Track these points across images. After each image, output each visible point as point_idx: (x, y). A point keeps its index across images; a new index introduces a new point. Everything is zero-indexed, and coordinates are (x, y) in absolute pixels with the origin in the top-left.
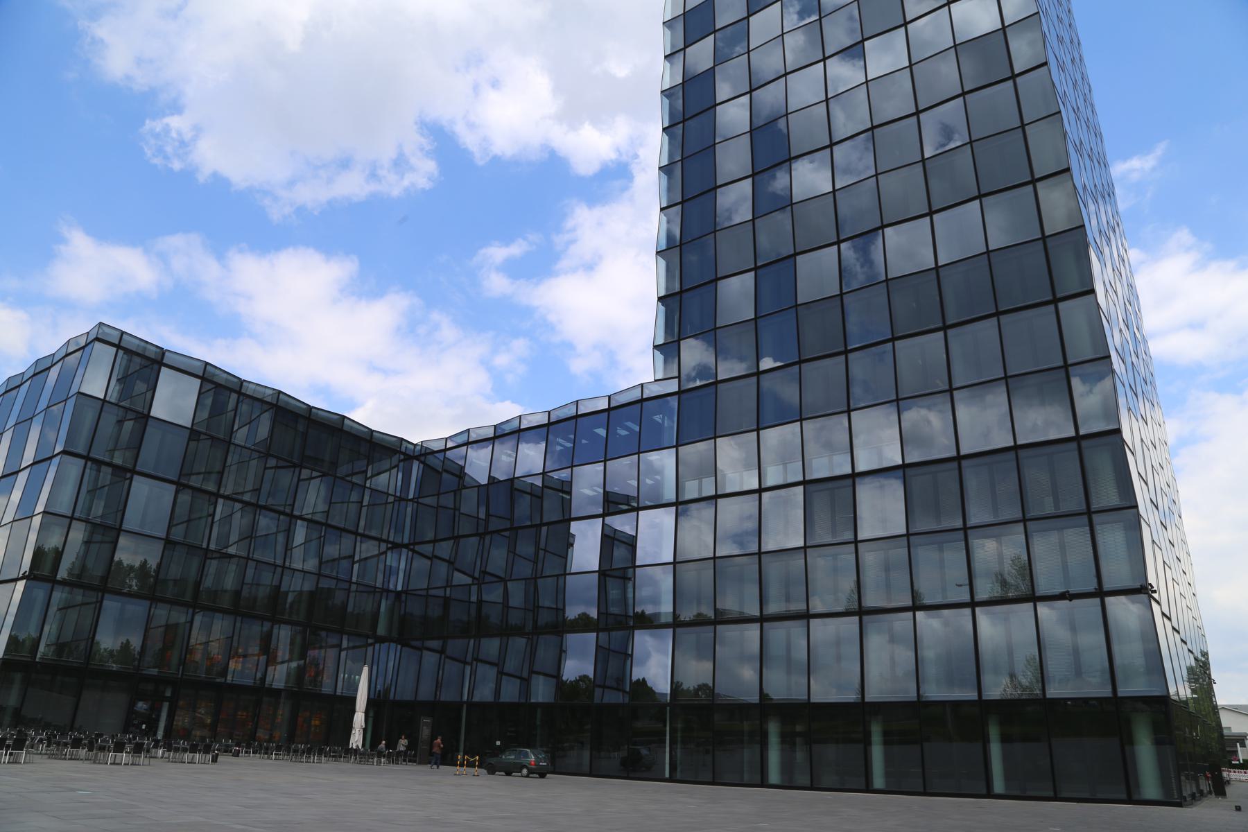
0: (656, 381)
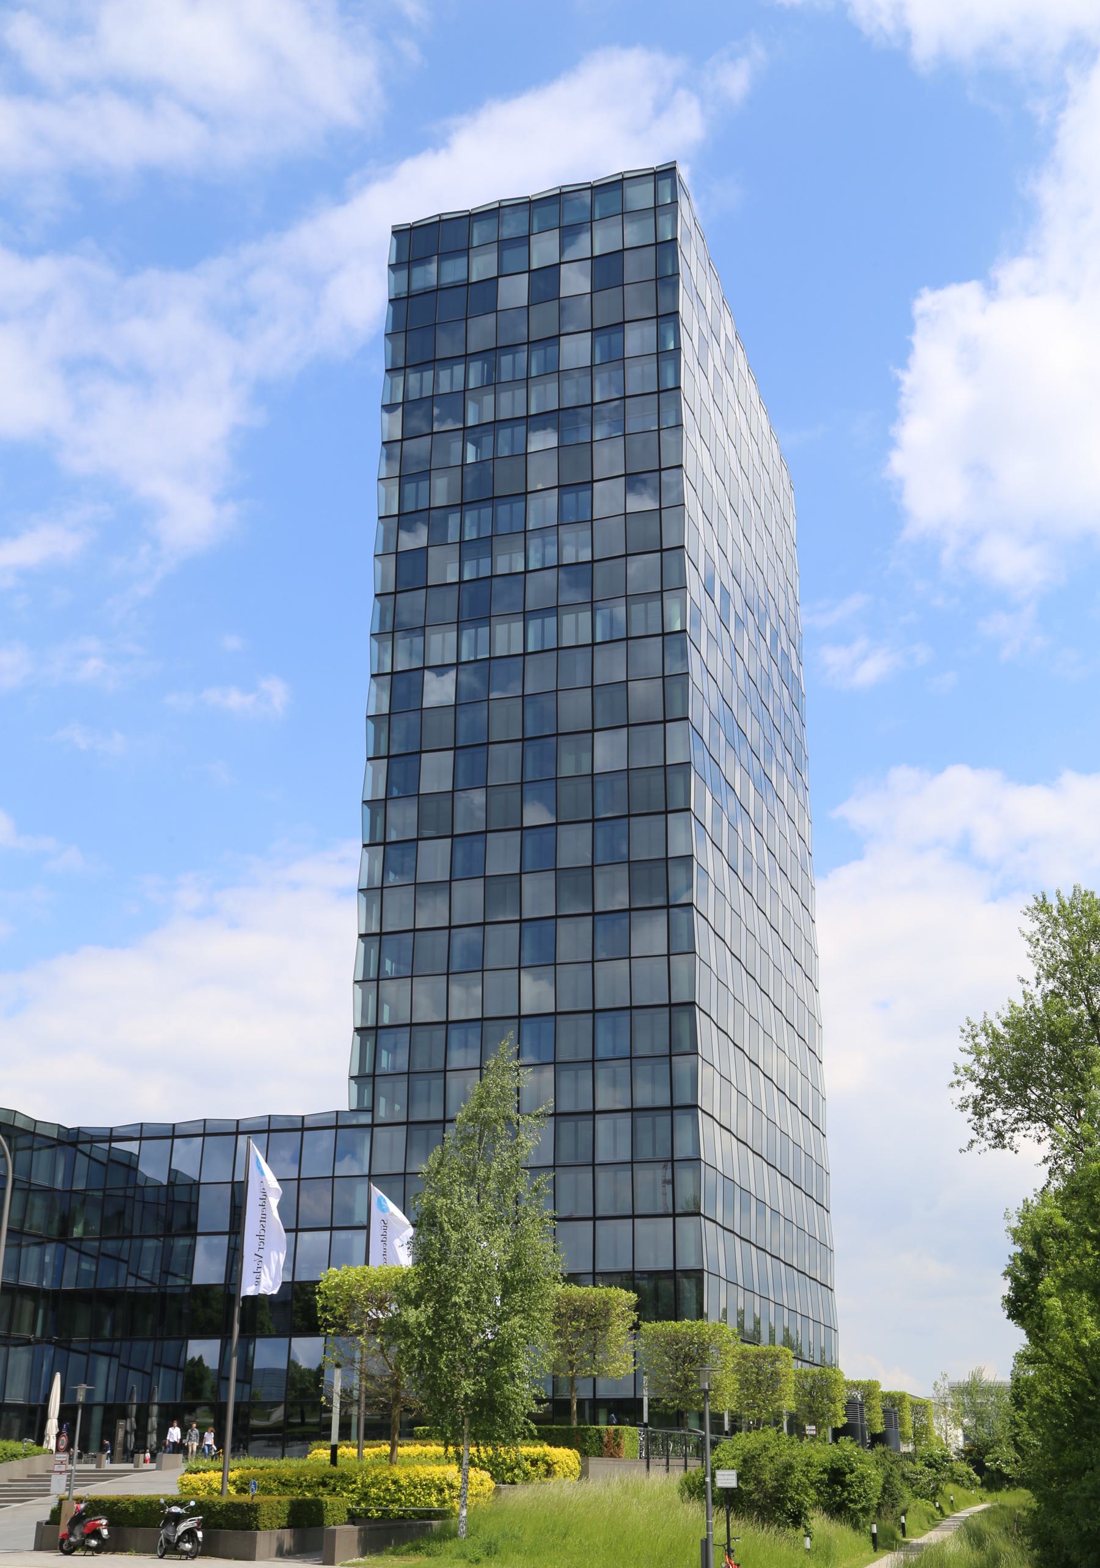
0: (351, 1110)
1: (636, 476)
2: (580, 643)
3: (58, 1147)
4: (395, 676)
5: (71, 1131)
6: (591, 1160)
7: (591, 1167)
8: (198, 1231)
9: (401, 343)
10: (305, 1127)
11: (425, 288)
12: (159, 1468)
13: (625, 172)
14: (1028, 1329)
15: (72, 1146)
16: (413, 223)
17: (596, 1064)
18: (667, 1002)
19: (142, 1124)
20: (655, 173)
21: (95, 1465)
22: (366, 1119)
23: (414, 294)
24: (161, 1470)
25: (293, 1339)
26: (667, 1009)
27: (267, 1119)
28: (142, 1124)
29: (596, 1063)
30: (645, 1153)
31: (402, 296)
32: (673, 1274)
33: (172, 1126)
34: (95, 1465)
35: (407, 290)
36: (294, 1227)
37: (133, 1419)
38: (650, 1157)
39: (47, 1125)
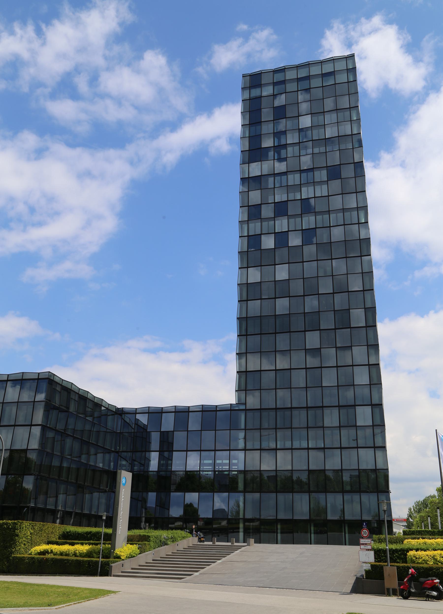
0: (236, 404)
1: (361, 163)
2: (338, 225)
3: (115, 415)
4: (249, 237)
5: (119, 409)
6: (291, 426)
7: (275, 430)
8: (174, 450)
9: (248, 116)
10: (163, 411)
11: (256, 96)
12: (249, 545)
13: (262, 70)
14: (145, 494)
15: (119, 415)
16: (251, 73)
17: (308, 389)
18: (305, 367)
19: (149, 407)
20: (297, 67)
21: (231, 543)
22: (243, 407)
23: (251, 98)
24: (250, 546)
25: (186, 493)
26: (336, 368)
27: (148, 408)
28: (149, 407)
29: (371, 385)
30: (265, 425)
31: (247, 99)
32: (375, 471)
33: (161, 408)
34: (231, 543)
35: (249, 97)
36: (186, 450)
37: (144, 523)
38: (251, 428)
39: (112, 406)
